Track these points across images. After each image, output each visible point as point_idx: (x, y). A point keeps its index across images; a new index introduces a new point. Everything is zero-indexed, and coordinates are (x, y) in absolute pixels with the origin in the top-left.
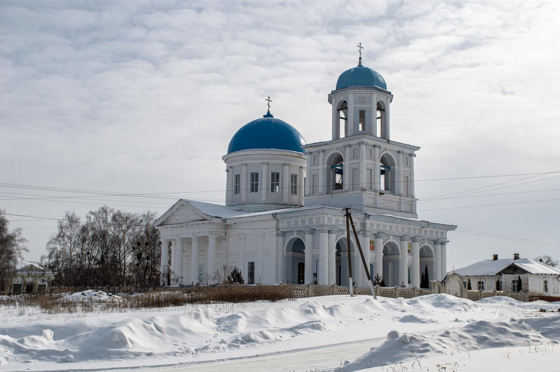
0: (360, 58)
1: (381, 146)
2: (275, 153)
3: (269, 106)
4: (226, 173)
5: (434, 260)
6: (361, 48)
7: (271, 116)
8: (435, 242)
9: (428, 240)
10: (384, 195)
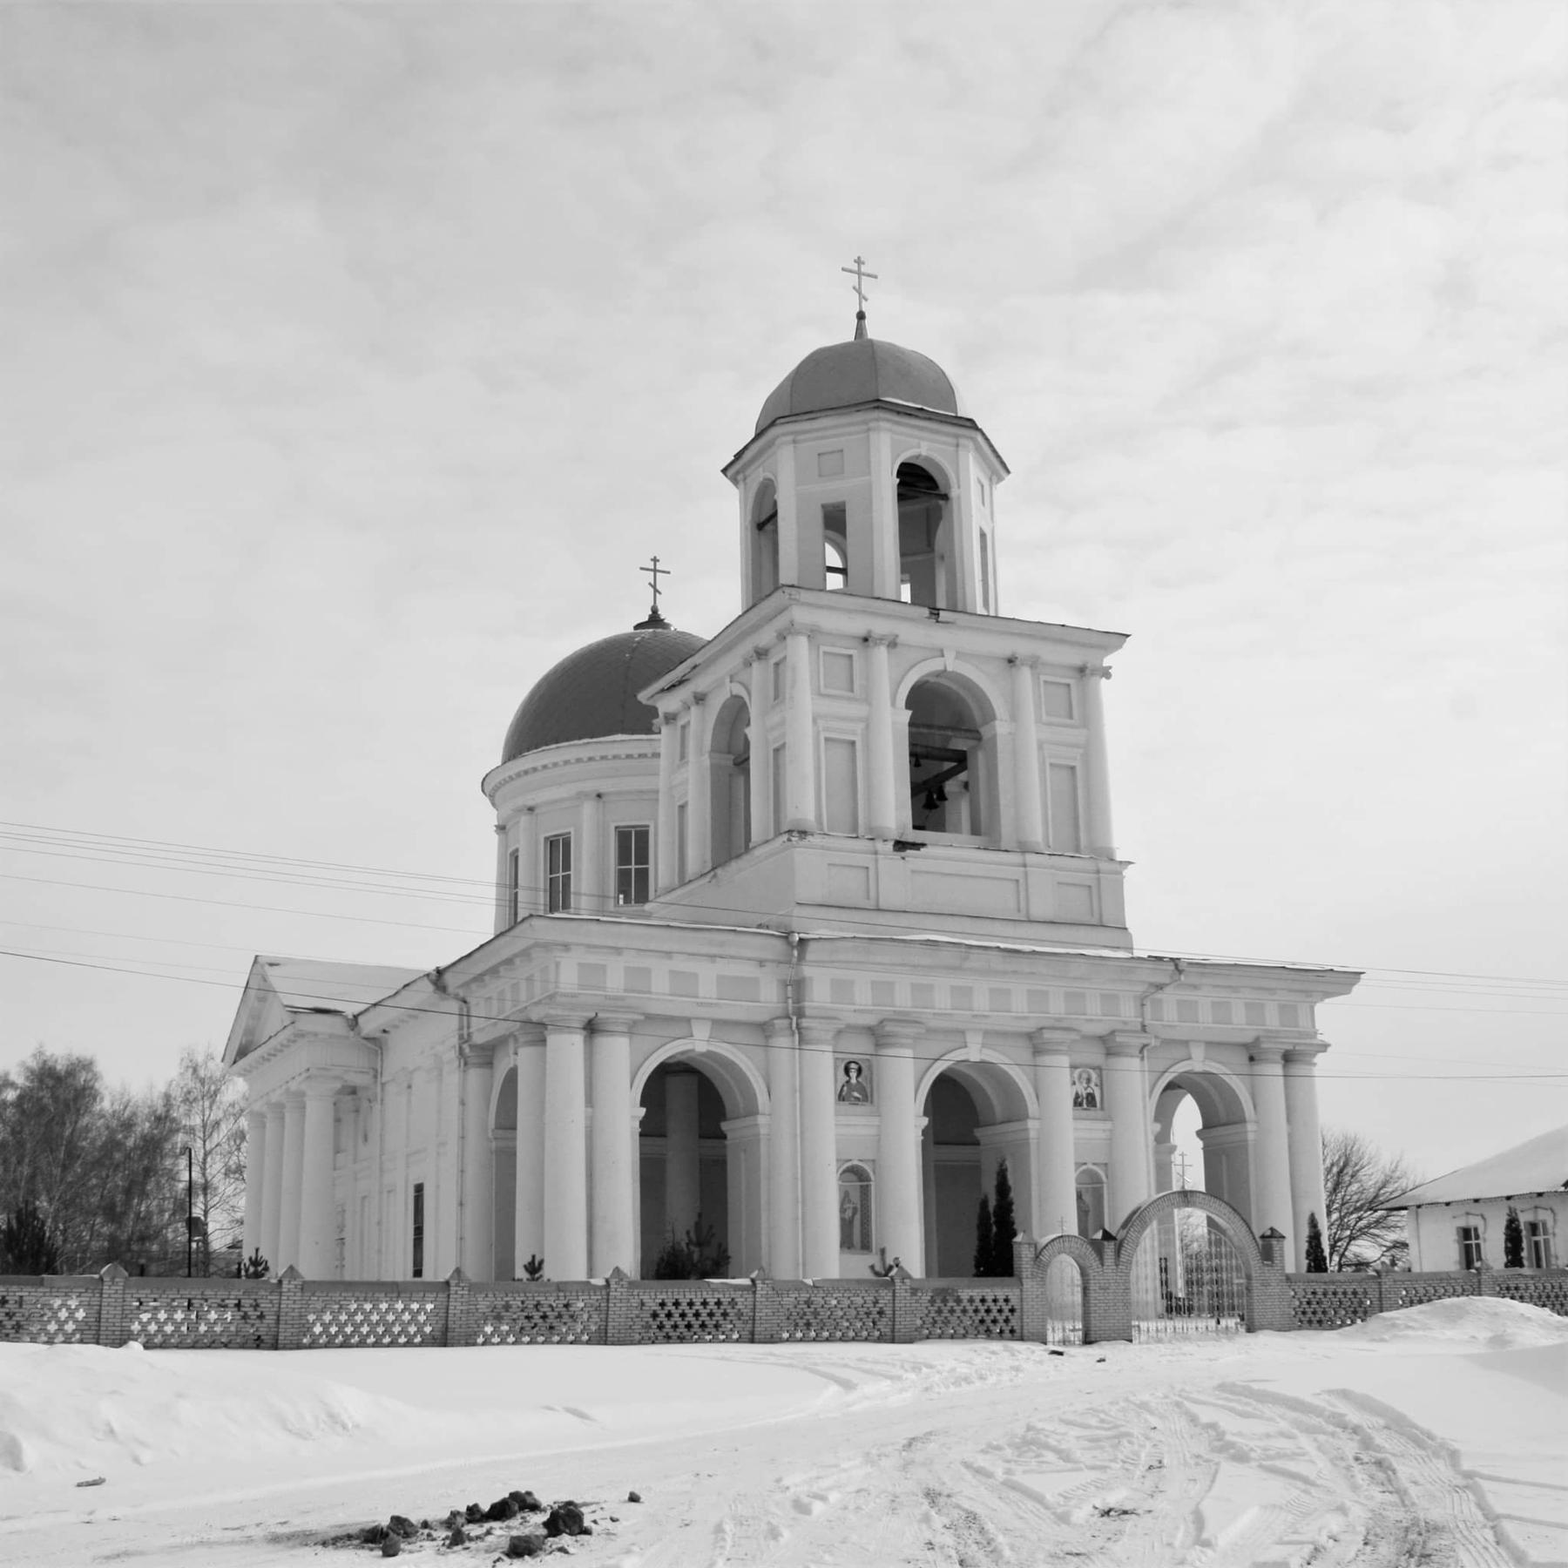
0: (861, 316)
1: (897, 636)
2: (622, 750)
3: (656, 591)
4: (497, 836)
5: (1251, 1136)
6: (863, 277)
7: (666, 626)
8: (1253, 1054)
9: (1210, 1044)
10: (923, 850)
